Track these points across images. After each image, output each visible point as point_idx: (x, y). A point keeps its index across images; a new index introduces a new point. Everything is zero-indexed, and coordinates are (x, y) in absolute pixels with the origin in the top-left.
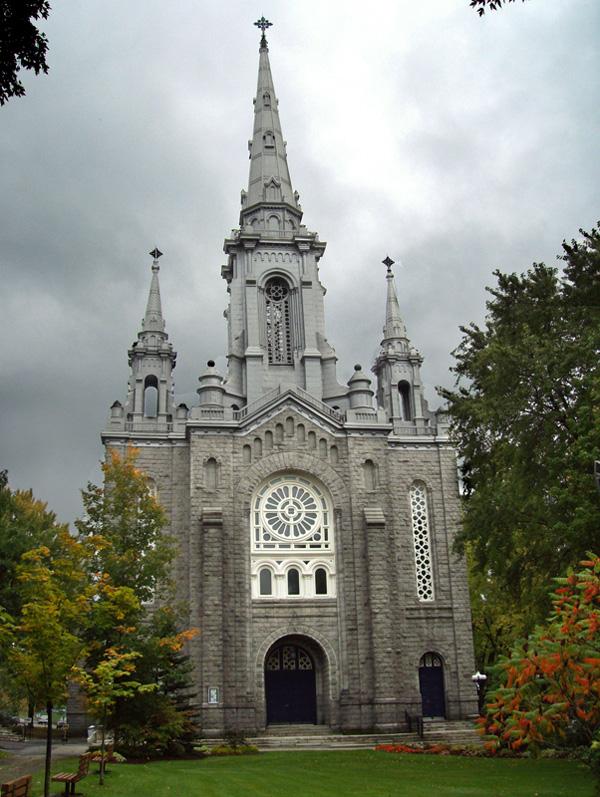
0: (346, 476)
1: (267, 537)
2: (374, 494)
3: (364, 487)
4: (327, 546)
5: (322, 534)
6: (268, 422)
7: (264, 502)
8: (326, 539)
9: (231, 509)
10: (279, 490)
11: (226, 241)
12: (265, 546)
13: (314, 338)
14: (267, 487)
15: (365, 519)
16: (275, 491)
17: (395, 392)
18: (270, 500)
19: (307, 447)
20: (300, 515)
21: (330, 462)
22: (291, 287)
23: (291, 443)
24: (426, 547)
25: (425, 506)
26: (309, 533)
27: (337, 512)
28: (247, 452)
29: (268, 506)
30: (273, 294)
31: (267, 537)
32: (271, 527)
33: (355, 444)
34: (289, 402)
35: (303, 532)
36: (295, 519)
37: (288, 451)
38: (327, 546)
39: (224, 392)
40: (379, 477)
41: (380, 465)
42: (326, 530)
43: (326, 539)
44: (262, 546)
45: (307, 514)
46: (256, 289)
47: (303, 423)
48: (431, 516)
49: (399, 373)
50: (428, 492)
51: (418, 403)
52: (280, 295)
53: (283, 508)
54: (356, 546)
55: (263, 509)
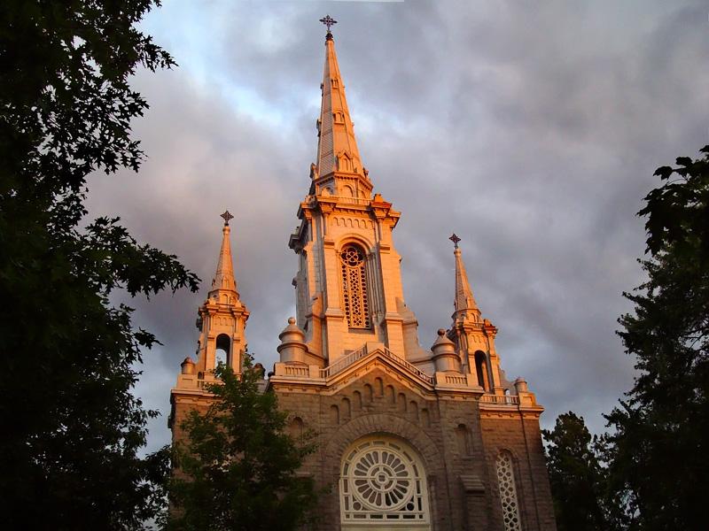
0: (439, 441)
1: (357, 506)
2: (469, 460)
3: (457, 453)
4: (421, 517)
5: (415, 503)
6: (355, 383)
7: (353, 468)
8: (420, 509)
9: (319, 474)
10: (369, 455)
11: (292, 235)
12: (356, 516)
13: (394, 302)
14: (368, 444)
15: (463, 487)
16: (364, 456)
17: (472, 361)
18: (363, 459)
19: (397, 409)
20: (391, 482)
21: (421, 426)
22: (367, 252)
23: (380, 405)
24: (515, 520)
25: (512, 477)
26: (402, 503)
27: (431, 479)
28: (334, 413)
29: (357, 473)
30: (349, 260)
31: (357, 506)
32: (361, 495)
33: (446, 408)
34: (377, 362)
35: (395, 501)
36: (386, 487)
37: (379, 413)
38: (421, 517)
39: (306, 350)
40: (472, 443)
41: (473, 430)
42: (419, 500)
43: (420, 509)
44: (352, 516)
45: (398, 482)
46: (334, 252)
47: (393, 384)
48: (519, 487)
49: (476, 343)
50: (514, 462)
51: (495, 372)
52: (356, 260)
53: (373, 474)
54: (454, 516)
55: (352, 476)
